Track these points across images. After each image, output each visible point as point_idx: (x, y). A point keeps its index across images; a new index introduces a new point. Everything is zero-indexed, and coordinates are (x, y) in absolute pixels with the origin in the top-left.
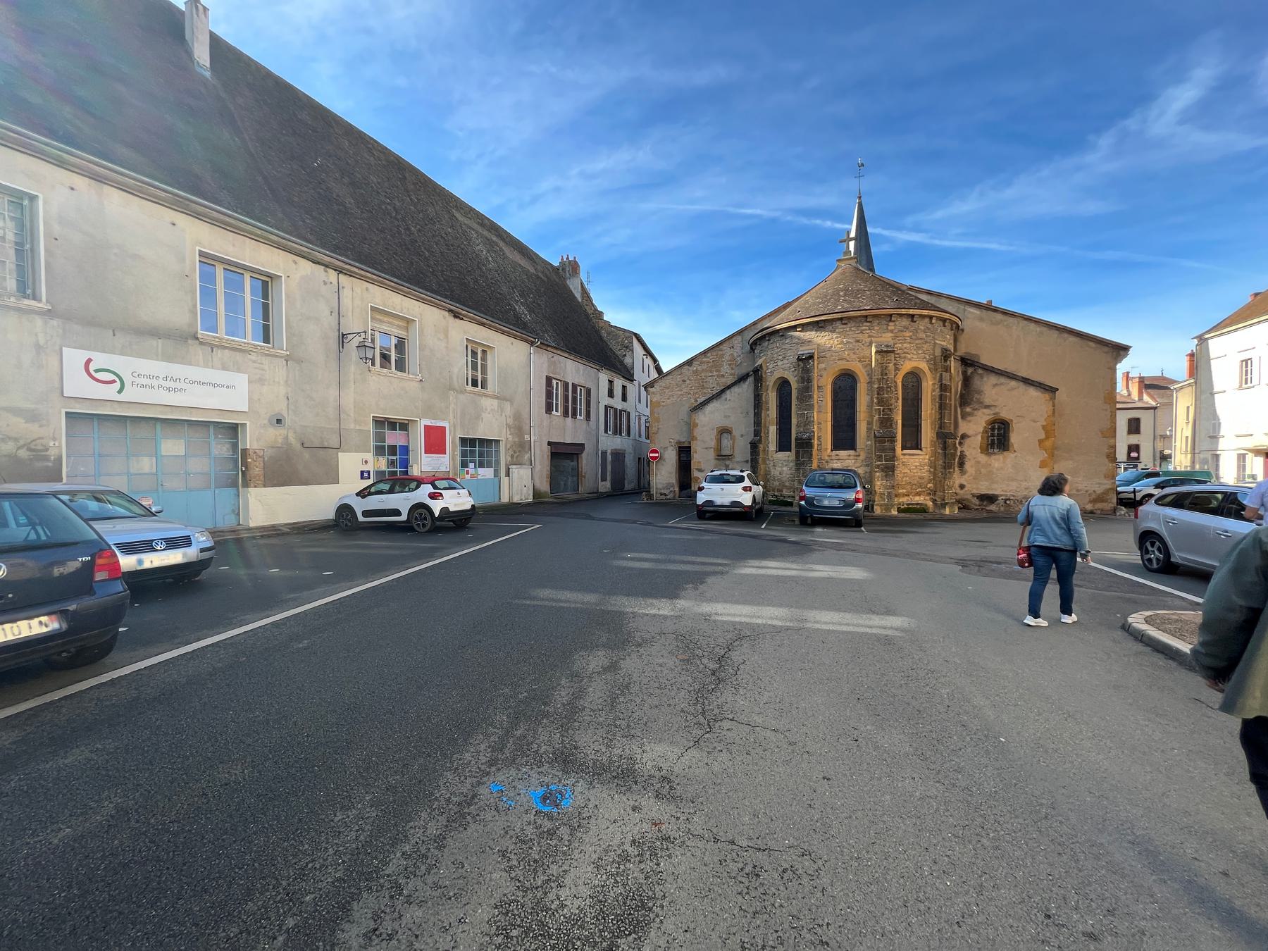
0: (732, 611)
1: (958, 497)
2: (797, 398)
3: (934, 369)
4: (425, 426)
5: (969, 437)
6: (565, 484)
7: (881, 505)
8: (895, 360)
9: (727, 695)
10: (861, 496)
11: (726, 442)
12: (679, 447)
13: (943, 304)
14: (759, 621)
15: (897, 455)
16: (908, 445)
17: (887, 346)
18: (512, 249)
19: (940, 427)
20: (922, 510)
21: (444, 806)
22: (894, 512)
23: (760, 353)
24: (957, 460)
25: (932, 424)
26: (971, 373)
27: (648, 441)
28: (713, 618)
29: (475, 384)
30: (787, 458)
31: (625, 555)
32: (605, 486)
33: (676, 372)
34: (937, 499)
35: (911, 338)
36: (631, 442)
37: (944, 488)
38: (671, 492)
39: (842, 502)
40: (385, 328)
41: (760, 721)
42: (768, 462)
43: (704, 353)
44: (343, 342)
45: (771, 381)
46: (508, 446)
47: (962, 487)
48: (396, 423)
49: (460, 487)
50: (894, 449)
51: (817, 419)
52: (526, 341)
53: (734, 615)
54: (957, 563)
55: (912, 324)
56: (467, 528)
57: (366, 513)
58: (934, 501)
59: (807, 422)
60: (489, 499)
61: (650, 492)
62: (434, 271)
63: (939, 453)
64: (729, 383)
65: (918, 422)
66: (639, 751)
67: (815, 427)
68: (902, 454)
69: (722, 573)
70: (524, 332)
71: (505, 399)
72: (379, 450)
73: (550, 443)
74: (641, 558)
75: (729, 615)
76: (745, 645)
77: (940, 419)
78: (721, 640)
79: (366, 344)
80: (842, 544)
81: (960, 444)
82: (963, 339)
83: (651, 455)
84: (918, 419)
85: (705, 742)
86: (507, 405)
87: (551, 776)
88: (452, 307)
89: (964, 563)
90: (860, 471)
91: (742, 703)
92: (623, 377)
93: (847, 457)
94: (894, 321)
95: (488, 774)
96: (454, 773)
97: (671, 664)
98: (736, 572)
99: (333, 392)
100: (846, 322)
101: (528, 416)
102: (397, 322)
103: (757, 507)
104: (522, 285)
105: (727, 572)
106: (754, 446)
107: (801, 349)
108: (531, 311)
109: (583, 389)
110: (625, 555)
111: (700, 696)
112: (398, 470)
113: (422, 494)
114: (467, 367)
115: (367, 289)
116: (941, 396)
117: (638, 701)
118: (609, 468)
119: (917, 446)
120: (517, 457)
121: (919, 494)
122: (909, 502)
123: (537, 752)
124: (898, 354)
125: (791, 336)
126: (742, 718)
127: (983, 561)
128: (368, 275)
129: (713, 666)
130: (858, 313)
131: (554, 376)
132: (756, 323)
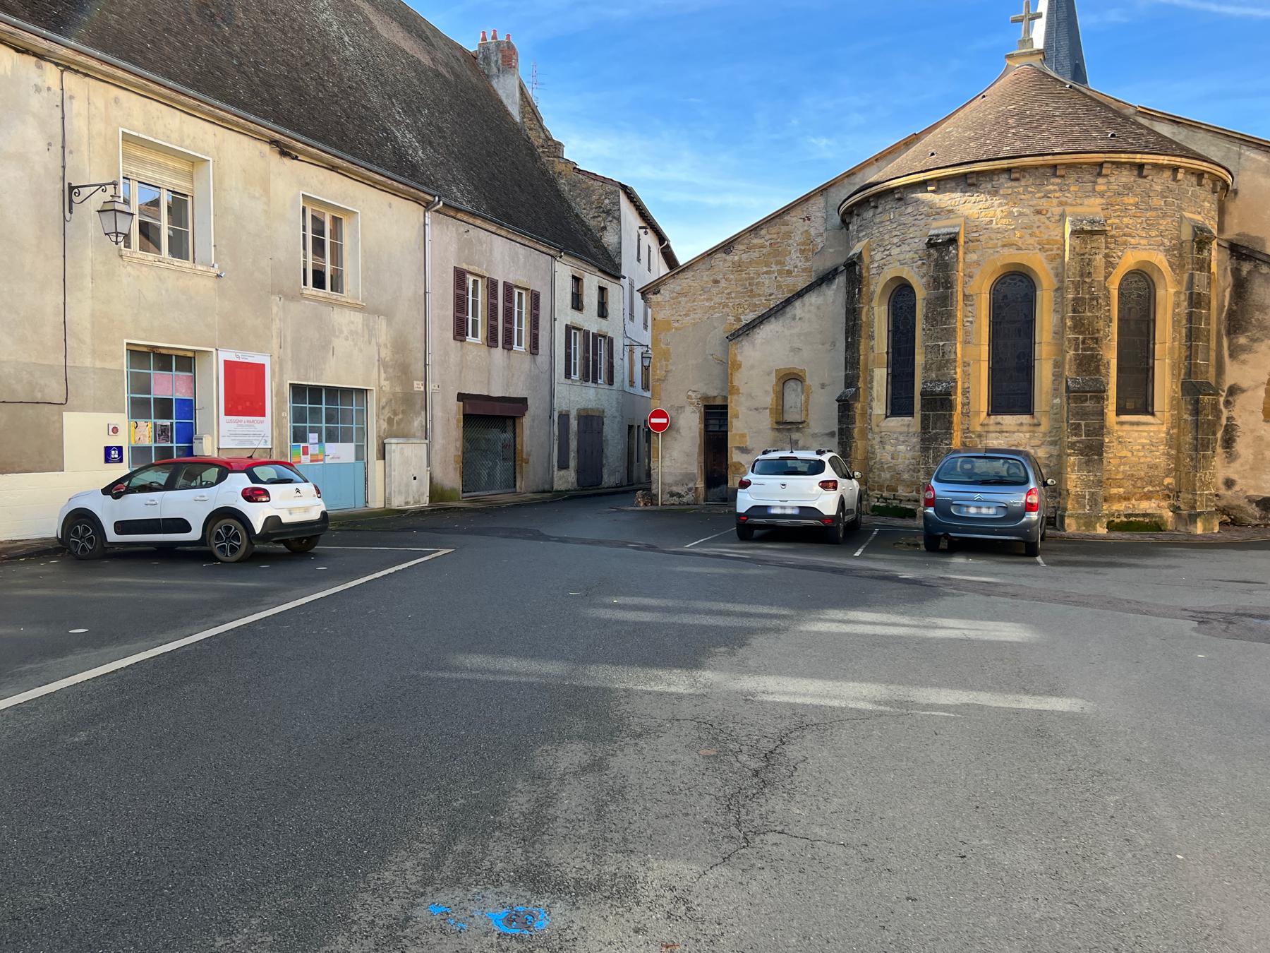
0: (791, 689)
1: (1222, 503)
2: (926, 317)
3: (1177, 266)
4: (225, 361)
5: (1243, 391)
6: (489, 475)
7: (1078, 517)
8: (1107, 248)
9: (776, 803)
10: (1034, 499)
11: (793, 397)
12: (706, 407)
13: (1200, 143)
14: (836, 703)
15: (1107, 424)
16: (1129, 405)
17: (1093, 222)
18: (388, 19)
19: (1189, 373)
20: (1155, 526)
21: (368, 930)
22: (1101, 530)
23: (858, 231)
24: (1219, 435)
25: (1173, 367)
26: (1249, 272)
27: (648, 394)
28: (758, 698)
29: (319, 282)
30: (905, 429)
31: (607, 600)
32: (566, 479)
33: (701, 266)
34: (1182, 506)
35: (1137, 205)
36: (614, 395)
37: (1195, 485)
38: (690, 490)
39: (1001, 509)
40: (149, 174)
41: (823, 834)
42: (870, 436)
43: (755, 229)
44: (71, 201)
45: (877, 283)
46: (384, 401)
47: (1229, 483)
48: (171, 355)
49: (300, 479)
50: (1101, 414)
51: (962, 356)
52: (416, 200)
53: (794, 694)
54: (1193, 618)
55: (1140, 181)
56: (313, 554)
57: (122, 527)
58: (1176, 510)
59: (943, 362)
60: (349, 503)
61: (649, 489)
62: (241, 64)
63: (1186, 421)
64: (801, 285)
65: (1148, 364)
66: (641, 869)
67: (958, 370)
68: (1117, 423)
69: (777, 630)
70: (413, 184)
71: (377, 312)
72: (139, 408)
73: (461, 397)
74: (634, 605)
75: (785, 693)
76: (809, 737)
77: (1189, 357)
78: (770, 730)
79: (118, 207)
80: (996, 584)
81: (1227, 403)
82: (1234, 208)
83: (653, 420)
84: (1148, 358)
85: (739, 858)
86: (381, 324)
87: (519, 898)
88: (278, 136)
89: (1203, 618)
90: (1041, 453)
91: (798, 812)
92: (601, 270)
93: (1016, 429)
94: (1107, 175)
95: (423, 894)
96: (373, 894)
97: (688, 761)
98: (802, 628)
99: (53, 298)
100: (1017, 175)
101: (420, 346)
102: (171, 163)
103: (847, 518)
104: (408, 91)
105: (786, 629)
106: (845, 406)
107: (935, 224)
108: (425, 141)
109: (524, 292)
110: (607, 600)
111: (733, 802)
112: (175, 445)
113: (231, 491)
114: (304, 248)
115: (116, 100)
116: (1190, 317)
117: (638, 809)
118: (573, 445)
119: (1146, 407)
120: (398, 423)
121: (1148, 497)
122: (1130, 512)
123: (491, 870)
124: (1112, 237)
125: (917, 200)
126: (795, 830)
127: (1238, 614)
128: (120, 73)
129: (753, 764)
130: (1039, 160)
131: (471, 268)
132: (853, 174)
